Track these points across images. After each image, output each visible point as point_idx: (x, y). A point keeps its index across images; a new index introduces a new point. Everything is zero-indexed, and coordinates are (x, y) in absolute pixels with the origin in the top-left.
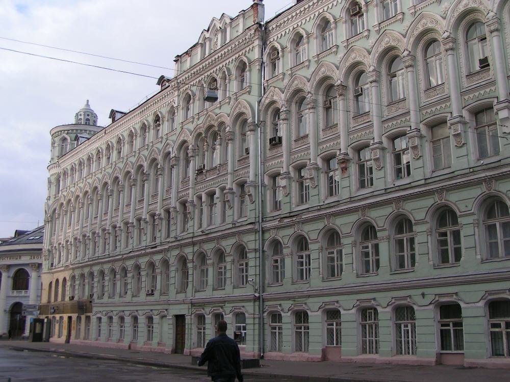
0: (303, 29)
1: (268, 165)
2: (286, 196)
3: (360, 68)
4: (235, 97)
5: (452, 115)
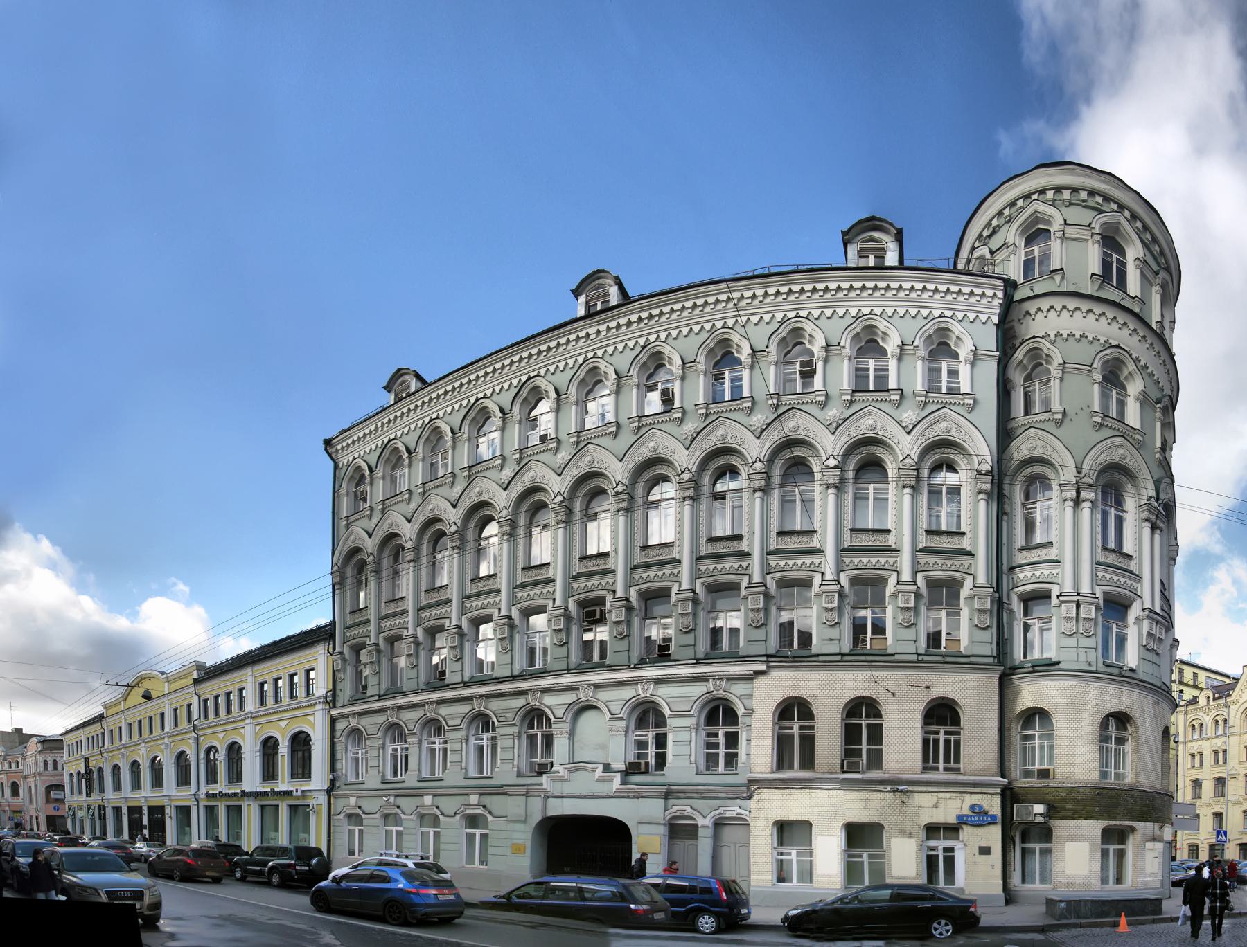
3: (600, 483)
4: (467, 473)
5: (680, 586)
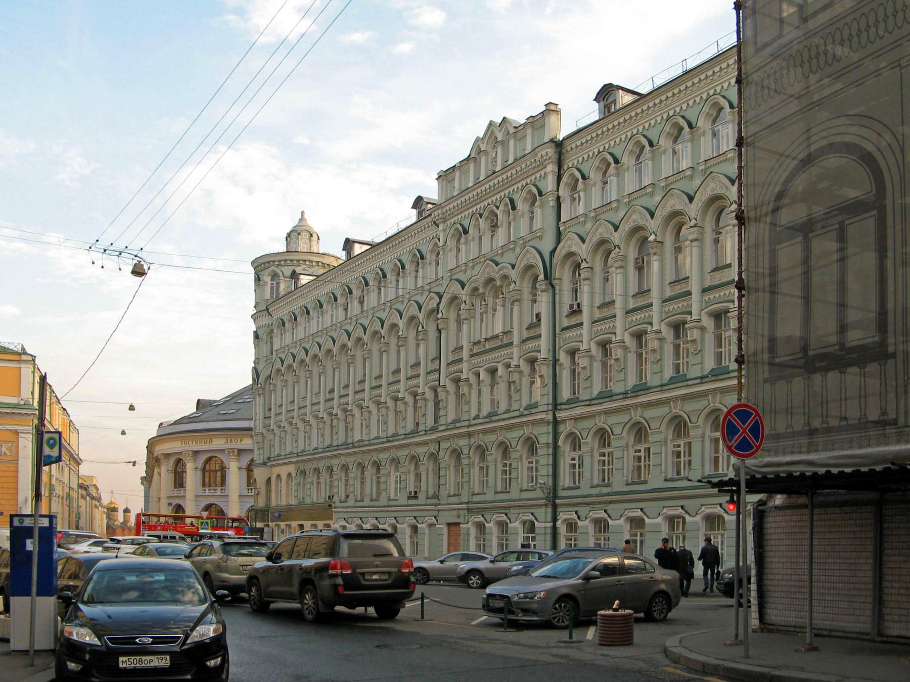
0: (724, 97)
1: (564, 337)
2: (620, 371)
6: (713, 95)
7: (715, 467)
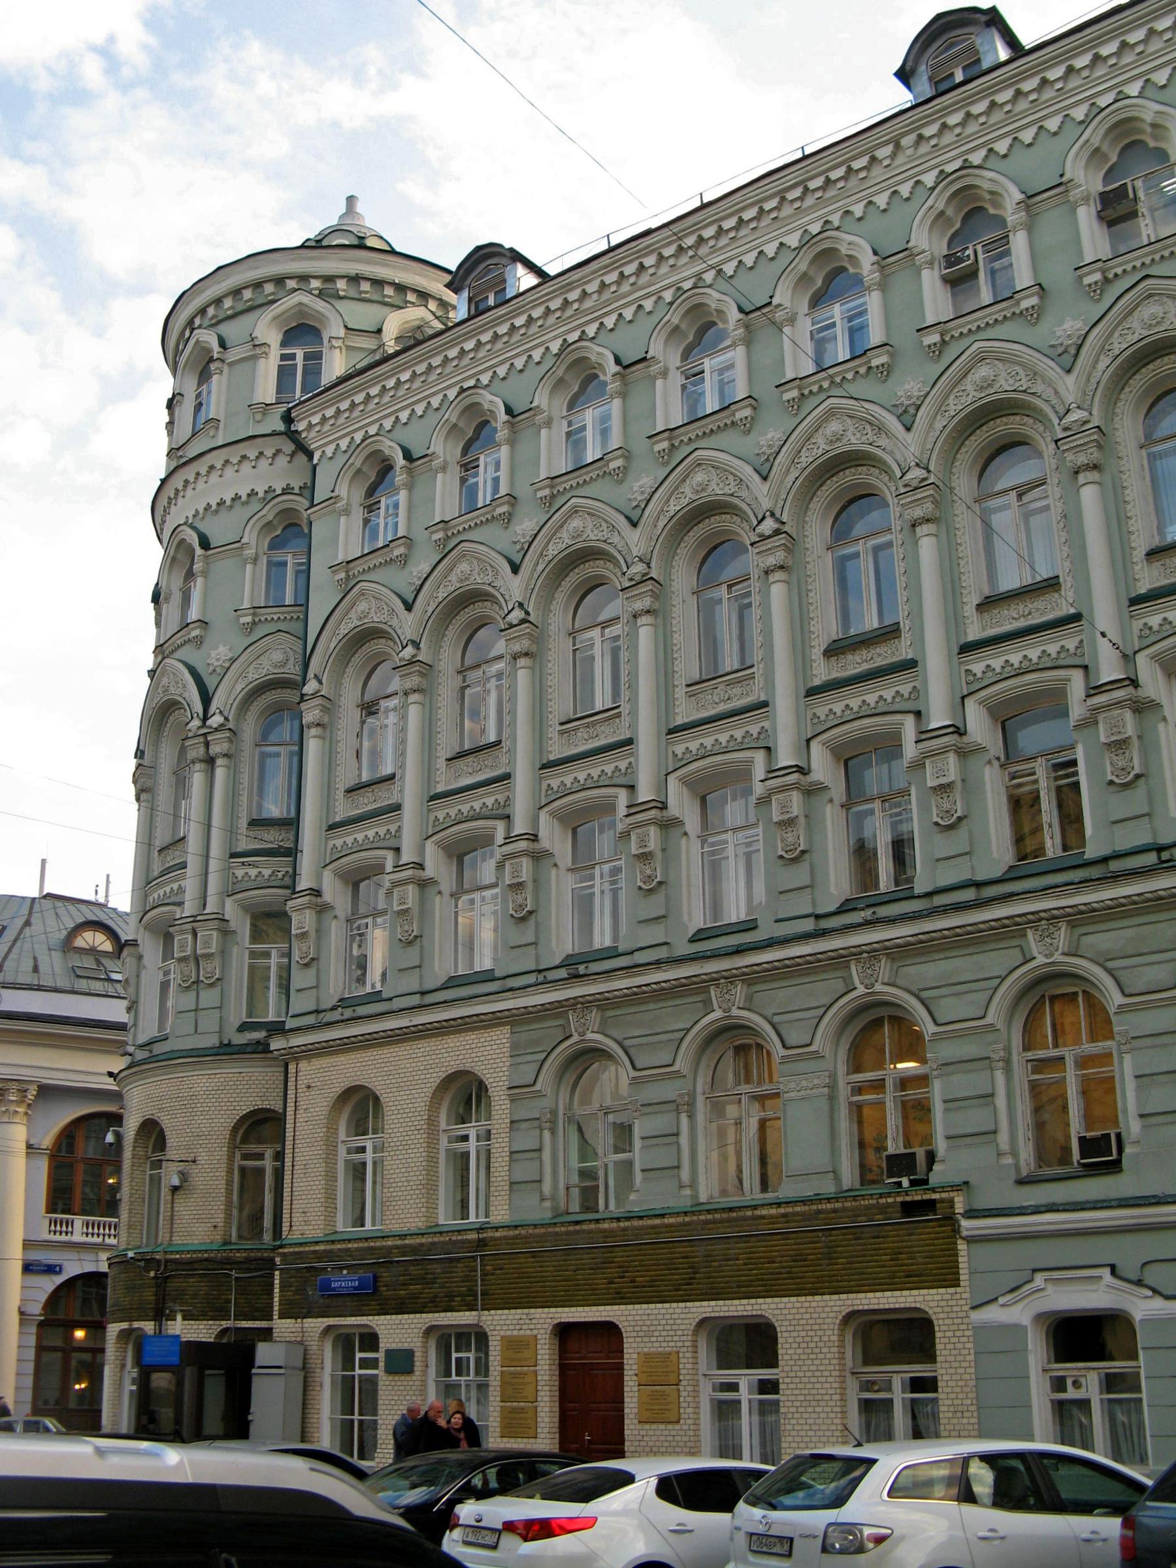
3: (872, 477)
5: (509, 829)
6: (377, 434)
7: (462, 1212)
